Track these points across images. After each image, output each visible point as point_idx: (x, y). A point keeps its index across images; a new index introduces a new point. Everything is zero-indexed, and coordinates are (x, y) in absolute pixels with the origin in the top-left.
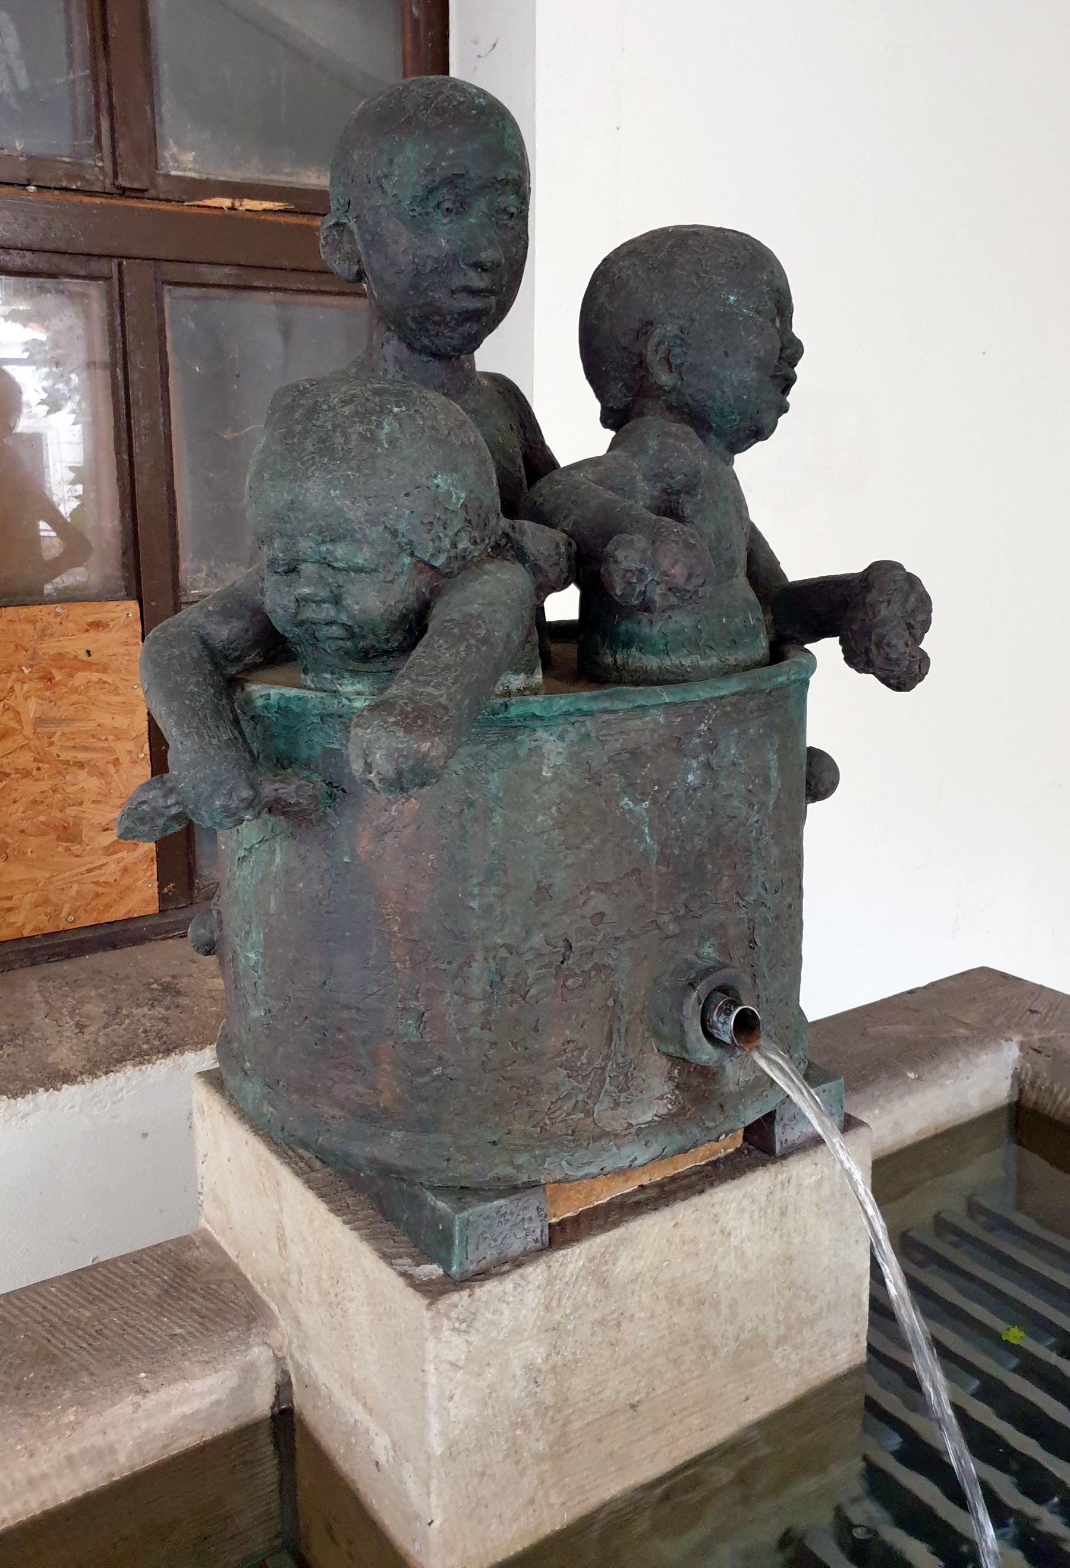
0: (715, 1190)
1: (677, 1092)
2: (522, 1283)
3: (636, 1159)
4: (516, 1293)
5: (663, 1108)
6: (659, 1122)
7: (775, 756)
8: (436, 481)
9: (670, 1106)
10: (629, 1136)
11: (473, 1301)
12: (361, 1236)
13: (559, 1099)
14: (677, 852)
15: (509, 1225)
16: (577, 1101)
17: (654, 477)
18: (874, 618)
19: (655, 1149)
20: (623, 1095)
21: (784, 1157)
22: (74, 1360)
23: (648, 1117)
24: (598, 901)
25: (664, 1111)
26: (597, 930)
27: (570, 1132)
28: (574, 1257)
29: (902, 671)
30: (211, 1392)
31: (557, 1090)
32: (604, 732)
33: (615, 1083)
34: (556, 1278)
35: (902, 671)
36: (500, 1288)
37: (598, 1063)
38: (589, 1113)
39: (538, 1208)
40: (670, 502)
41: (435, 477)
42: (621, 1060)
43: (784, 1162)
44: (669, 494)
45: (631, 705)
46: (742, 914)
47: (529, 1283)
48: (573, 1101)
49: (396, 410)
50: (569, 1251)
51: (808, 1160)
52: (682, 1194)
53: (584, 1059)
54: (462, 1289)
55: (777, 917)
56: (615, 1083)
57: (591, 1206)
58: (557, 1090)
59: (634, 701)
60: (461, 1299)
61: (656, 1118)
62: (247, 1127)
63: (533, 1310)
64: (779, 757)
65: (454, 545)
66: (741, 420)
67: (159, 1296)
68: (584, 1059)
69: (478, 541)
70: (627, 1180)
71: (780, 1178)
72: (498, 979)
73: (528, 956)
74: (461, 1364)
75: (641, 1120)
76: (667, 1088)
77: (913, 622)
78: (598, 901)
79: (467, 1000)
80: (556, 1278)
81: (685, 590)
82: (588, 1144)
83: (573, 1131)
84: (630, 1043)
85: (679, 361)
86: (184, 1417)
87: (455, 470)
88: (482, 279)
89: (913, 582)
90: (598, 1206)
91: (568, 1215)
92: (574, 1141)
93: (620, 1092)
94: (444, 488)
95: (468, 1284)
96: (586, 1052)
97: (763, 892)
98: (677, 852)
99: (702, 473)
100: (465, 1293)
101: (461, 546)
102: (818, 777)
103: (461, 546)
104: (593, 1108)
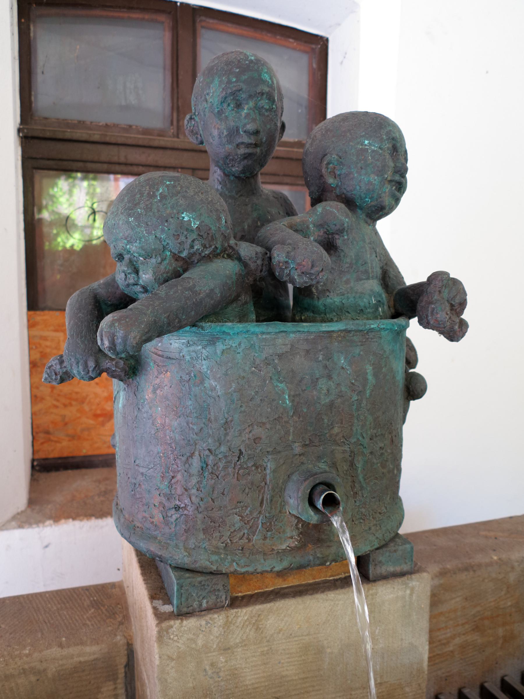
0: (330, 592)
1: (301, 536)
2: (210, 622)
3: (274, 567)
4: (207, 627)
5: (293, 543)
6: (290, 551)
7: (371, 368)
8: (183, 215)
9: (296, 543)
10: (272, 555)
11: (182, 626)
12: (147, 586)
13: (235, 531)
14: (305, 410)
15: (207, 591)
16: (244, 533)
17: (320, 226)
18: (438, 303)
19: (285, 564)
20: (269, 533)
21: (374, 581)
22: (39, 626)
23: (284, 547)
24: (258, 431)
25: (293, 545)
26: (257, 446)
27: (240, 548)
28: (243, 614)
29: (454, 330)
30: (94, 654)
31: (234, 526)
32: (264, 344)
33: (265, 526)
34: (231, 623)
35: (454, 330)
36: (198, 623)
37: (255, 514)
38: (249, 540)
39: (223, 585)
40: (329, 238)
41: (183, 213)
42: (267, 515)
43: (373, 584)
44: (328, 235)
45: (278, 331)
46: (346, 448)
47: (215, 623)
48: (242, 533)
49: (168, 183)
50: (240, 610)
51: (389, 586)
52: (311, 592)
53: (247, 512)
54: (178, 619)
55: (371, 453)
56: (265, 526)
57: (262, 591)
58: (234, 526)
59: (280, 329)
60: (175, 624)
61: (288, 548)
62: (63, 521)
63: (217, 637)
64: (373, 369)
65: (192, 247)
66: (371, 202)
67: (88, 606)
68: (247, 512)
69: (208, 246)
70: (285, 580)
71: (371, 592)
72: (205, 466)
73: (220, 456)
74: (174, 657)
75: (279, 548)
76: (295, 533)
77: (454, 303)
78: (258, 431)
79: (190, 475)
80: (231, 623)
81: (311, 273)
82: (249, 556)
83: (243, 548)
84: (273, 507)
85: (339, 173)
86: (80, 662)
87: (194, 211)
88: (250, 138)
89: (456, 283)
90: (266, 591)
91: (248, 593)
92: (242, 553)
93: (267, 531)
94: (186, 219)
95: (181, 617)
96: (249, 509)
97: (361, 438)
98: (305, 410)
99: (346, 225)
100: (178, 622)
101: (196, 247)
102: (414, 388)
103: (196, 247)
104: (253, 538)
